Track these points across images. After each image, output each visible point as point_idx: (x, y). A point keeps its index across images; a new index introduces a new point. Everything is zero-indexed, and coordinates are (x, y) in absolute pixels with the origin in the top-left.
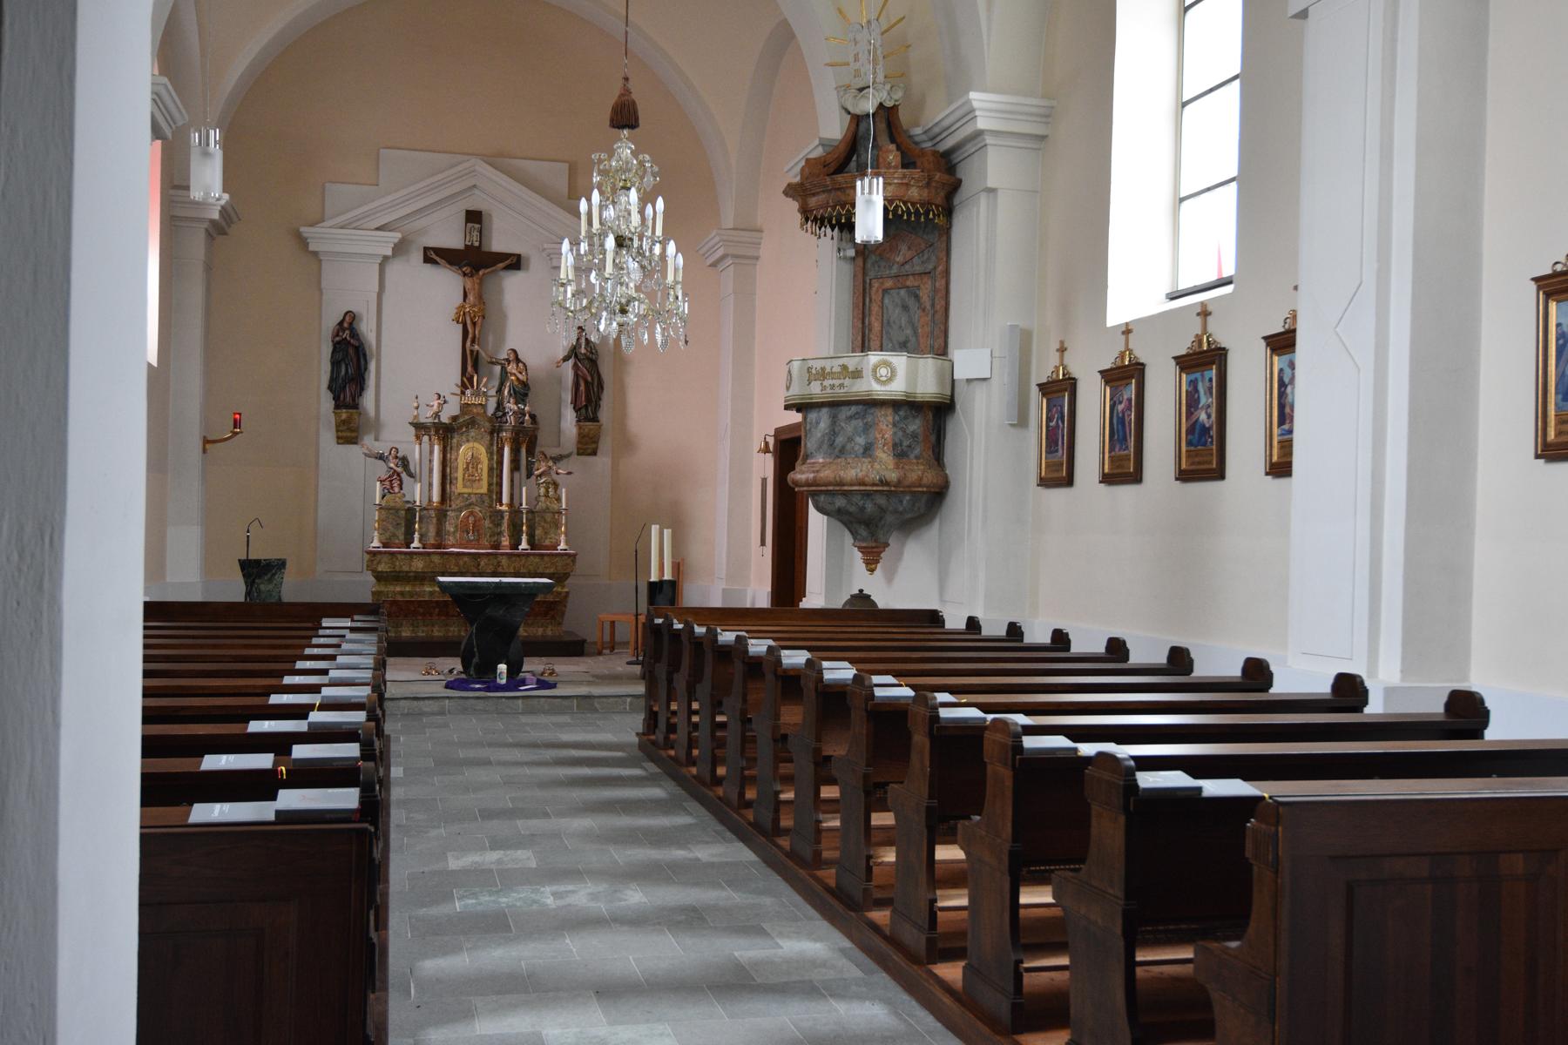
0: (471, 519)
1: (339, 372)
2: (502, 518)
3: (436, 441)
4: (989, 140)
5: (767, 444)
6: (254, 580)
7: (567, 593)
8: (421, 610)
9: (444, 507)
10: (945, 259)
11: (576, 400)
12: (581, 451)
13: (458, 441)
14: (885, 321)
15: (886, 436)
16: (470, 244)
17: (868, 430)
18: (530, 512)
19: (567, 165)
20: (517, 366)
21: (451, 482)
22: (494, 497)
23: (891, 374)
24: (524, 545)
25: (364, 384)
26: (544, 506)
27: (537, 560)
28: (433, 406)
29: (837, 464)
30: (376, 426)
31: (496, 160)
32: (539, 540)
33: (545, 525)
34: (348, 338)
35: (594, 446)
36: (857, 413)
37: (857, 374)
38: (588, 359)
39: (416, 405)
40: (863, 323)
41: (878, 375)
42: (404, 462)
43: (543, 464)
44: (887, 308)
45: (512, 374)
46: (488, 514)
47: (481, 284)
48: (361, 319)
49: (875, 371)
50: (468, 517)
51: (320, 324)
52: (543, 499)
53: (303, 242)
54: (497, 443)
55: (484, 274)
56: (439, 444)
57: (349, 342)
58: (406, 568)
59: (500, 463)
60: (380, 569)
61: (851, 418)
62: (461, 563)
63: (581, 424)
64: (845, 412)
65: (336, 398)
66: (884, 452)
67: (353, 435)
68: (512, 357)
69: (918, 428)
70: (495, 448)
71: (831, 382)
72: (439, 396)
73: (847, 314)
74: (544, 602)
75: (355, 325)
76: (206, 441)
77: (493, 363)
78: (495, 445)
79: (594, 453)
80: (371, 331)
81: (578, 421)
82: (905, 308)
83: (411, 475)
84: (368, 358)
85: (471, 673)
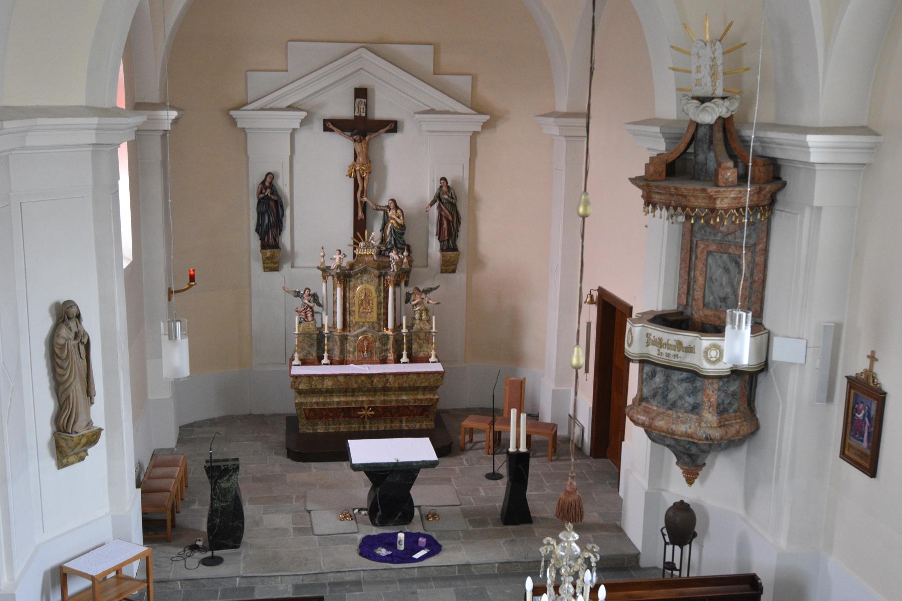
0: (365, 343)
1: (263, 221)
2: (388, 339)
3: (338, 285)
4: (817, 167)
5: (592, 297)
6: (217, 480)
7: (438, 400)
8: (331, 415)
9: (346, 333)
10: (765, 240)
11: (440, 232)
12: (443, 271)
13: (354, 284)
14: (708, 277)
15: (712, 400)
16: (358, 115)
17: (697, 392)
18: (409, 336)
19: (432, 46)
20: (396, 212)
21: (350, 314)
22: (382, 323)
23: (720, 355)
24: (404, 359)
25: (282, 226)
26: (419, 327)
27: (415, 377)
28: (335, 259)
29: (669, 416)
30: (291, 257)
31: (374, 46)
32: (415, 353)
33: (420, 341)
34: (269, 195)
35: (453, 267)
36: (687, 378)
37: (690, 350)
38: (449, 202)
39: (322, 254)
40: (689, 275)
41: (709, 356)
42: (315, 297)
43: (418, 296)
44: (711, 268)
45: (392, 219)
46: (378, 338)
47: (367, 148)
48: (278, 177)
49: (706, 352)
50: (364, 340)
51: (248, 181)
52: (418, 322)
53: (233, 121)
54: (384, 284)
55: (370, 139)
56: (341, 286)
57: (270, 198)
58: (319, 386)
59: (386, 298)
60: (300, 388)
61: (682, 380)
62: (359, 381)
63: (445, 253)
64: (676, 376)
65: (262, 239)
66: (710, 412)
67: (276, 266)
68: (392, 206)
69: (738, 388)
70: (382, 287)
71: (668, 351)
72: (340, 251)
73: (675, 264)
74: (421, 406)
75: (274, 183)
76: (170, 292)
77: (377, 210)
78: (382, 285)
79: (454, 271)
80: (286, 185)
81: (442, 250)
82: (727, 270)
83: (320, 305)
84: (284, 207)
85: (376, 522)
